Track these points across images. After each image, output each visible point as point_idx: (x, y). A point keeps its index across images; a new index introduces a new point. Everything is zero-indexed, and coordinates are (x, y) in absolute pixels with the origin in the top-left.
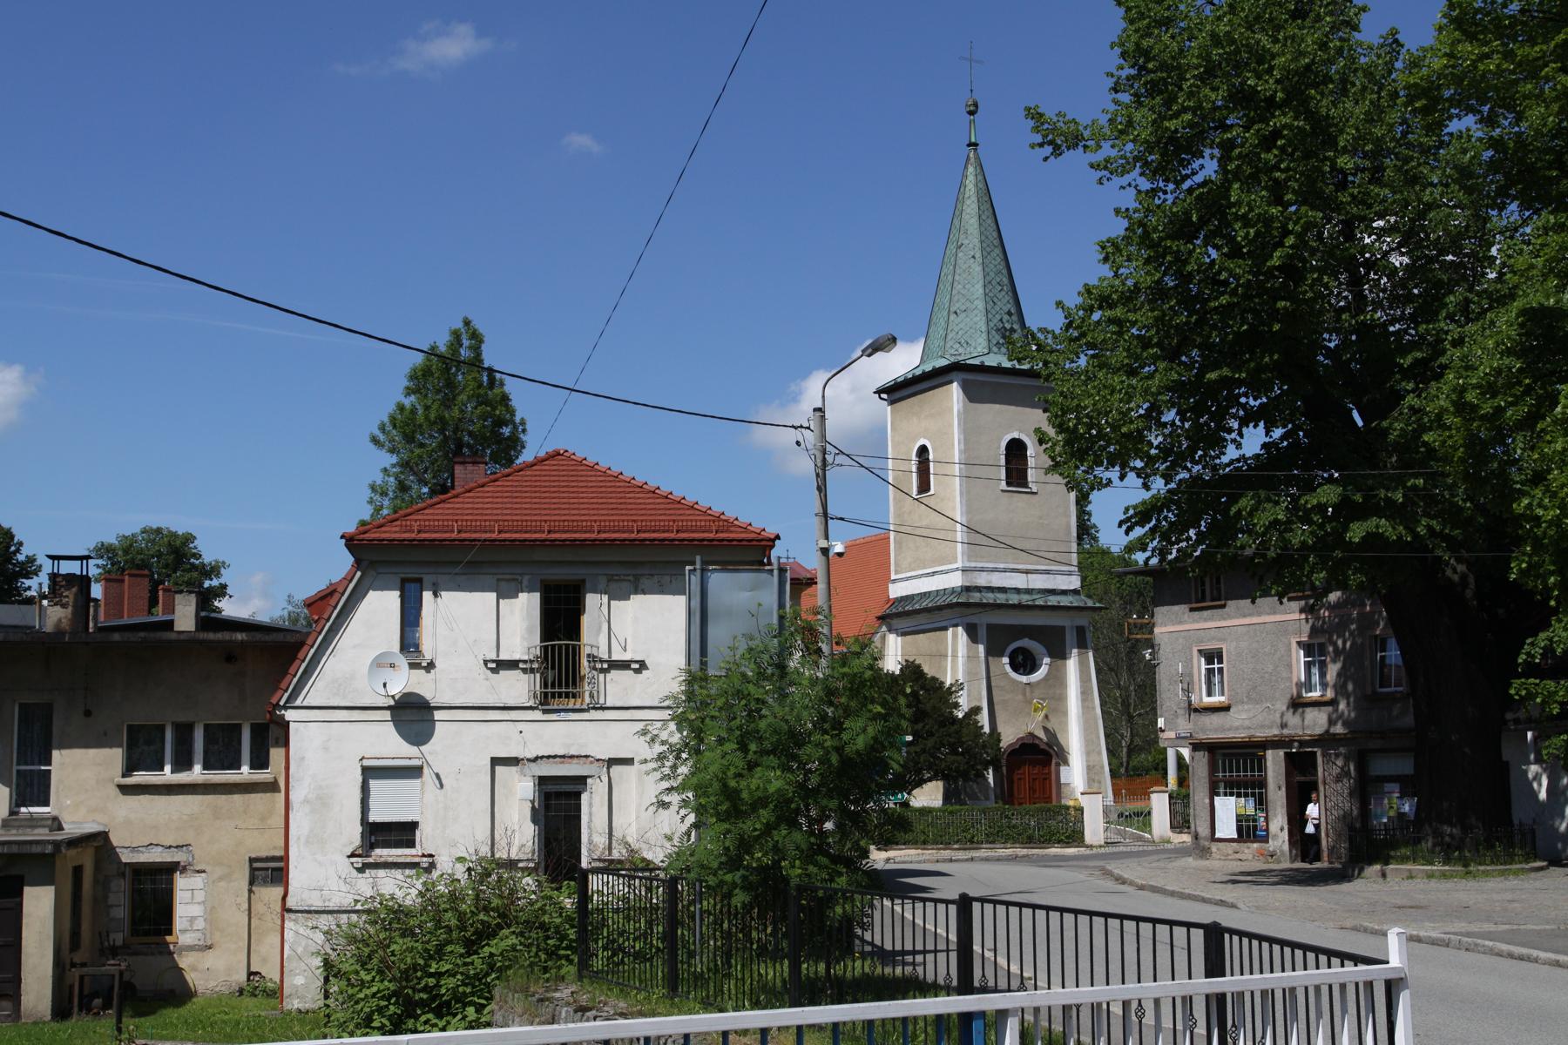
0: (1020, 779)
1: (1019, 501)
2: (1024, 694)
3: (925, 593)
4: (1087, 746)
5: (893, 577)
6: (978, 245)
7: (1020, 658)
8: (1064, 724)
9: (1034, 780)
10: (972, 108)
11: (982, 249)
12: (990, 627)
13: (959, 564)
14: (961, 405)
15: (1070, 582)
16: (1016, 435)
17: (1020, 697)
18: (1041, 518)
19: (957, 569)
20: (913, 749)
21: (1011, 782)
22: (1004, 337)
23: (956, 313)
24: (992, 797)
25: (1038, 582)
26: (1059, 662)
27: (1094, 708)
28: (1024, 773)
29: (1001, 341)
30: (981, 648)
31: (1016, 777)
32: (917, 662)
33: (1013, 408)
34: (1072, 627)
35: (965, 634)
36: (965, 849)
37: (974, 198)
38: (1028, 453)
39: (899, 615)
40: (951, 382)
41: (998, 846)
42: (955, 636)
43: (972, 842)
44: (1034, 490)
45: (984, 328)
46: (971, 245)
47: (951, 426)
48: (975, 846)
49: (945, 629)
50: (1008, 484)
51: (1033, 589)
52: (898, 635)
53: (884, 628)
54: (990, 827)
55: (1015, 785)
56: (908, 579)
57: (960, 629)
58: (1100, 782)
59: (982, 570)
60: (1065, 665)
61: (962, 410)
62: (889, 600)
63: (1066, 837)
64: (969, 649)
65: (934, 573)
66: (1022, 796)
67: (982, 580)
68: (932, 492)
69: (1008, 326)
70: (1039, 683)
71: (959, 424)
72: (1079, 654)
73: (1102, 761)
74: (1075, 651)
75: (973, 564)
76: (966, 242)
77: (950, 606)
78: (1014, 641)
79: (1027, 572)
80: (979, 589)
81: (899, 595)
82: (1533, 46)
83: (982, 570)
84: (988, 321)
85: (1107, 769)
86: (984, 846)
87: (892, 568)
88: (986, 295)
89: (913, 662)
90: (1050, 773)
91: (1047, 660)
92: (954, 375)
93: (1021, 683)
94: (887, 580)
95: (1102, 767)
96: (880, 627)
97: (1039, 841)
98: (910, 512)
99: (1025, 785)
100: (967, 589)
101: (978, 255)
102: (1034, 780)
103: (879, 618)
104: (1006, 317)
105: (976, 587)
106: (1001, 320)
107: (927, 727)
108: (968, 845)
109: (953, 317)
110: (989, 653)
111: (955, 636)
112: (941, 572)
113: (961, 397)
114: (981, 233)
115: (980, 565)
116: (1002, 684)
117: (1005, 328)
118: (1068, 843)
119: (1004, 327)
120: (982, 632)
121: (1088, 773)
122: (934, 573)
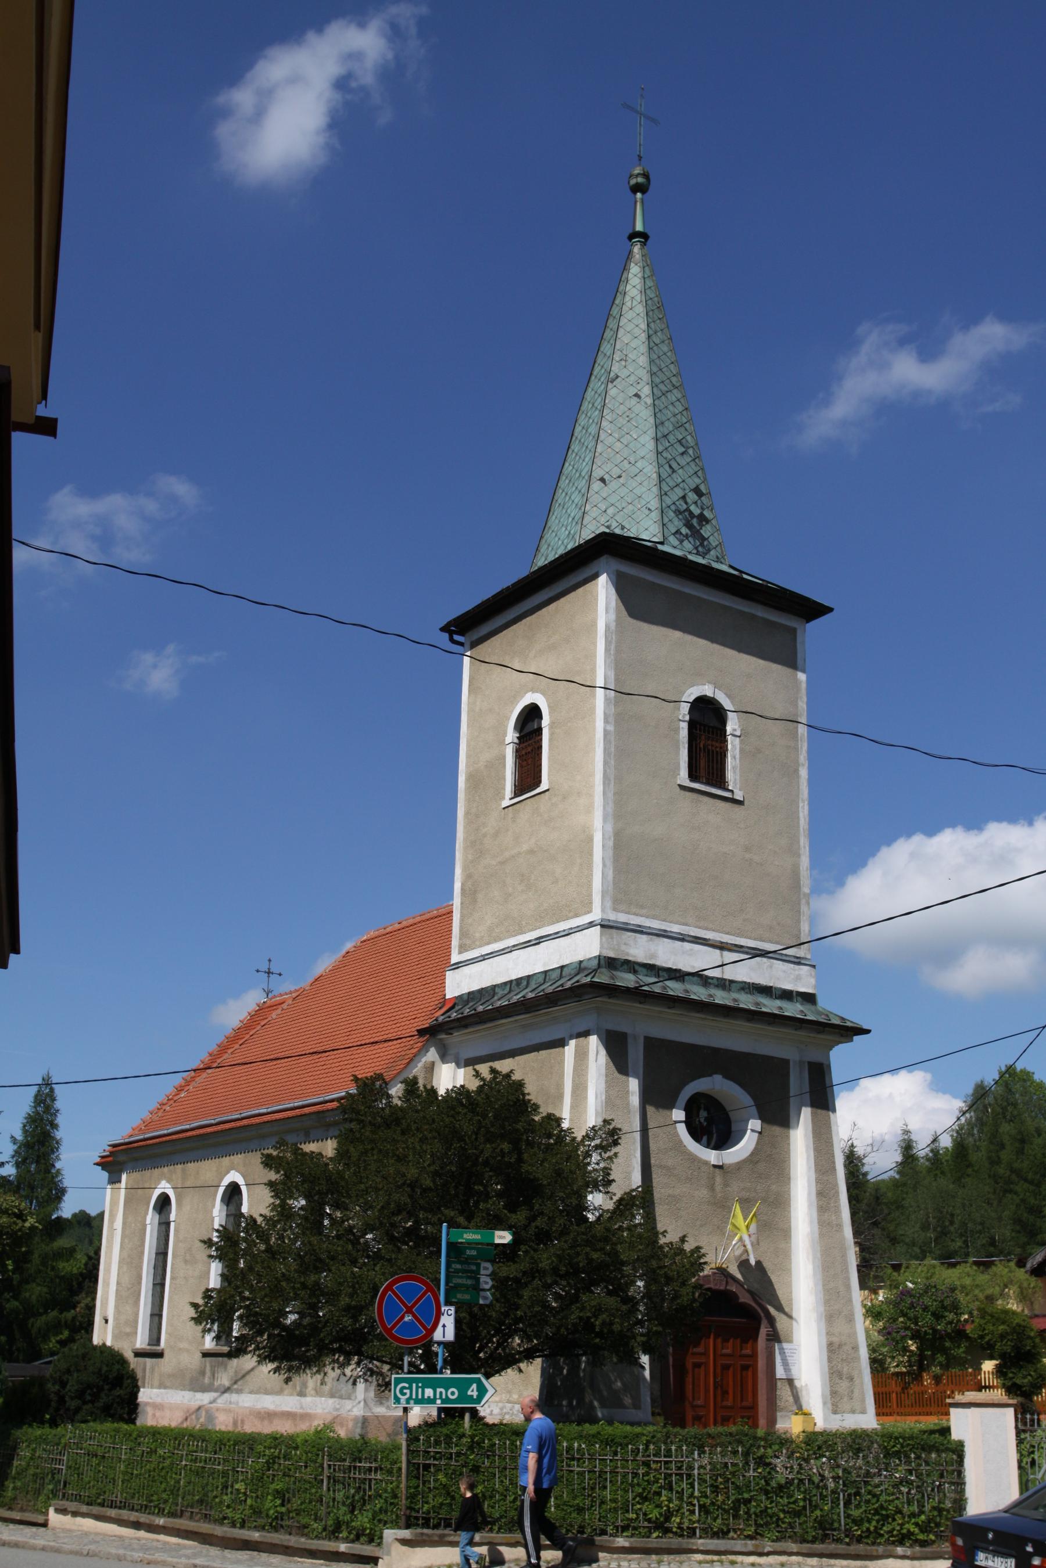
0: (697, 1365)
1: (710, 812)
2: (712, 1188)
3: (519, 981)
4: (827, 1302)
5: (455, 958)
6: (646, 377)
7: (703, 1114)
8: (785, 1255)
9: (726, 1368)
10: (640, 180)
11: (654, 385)
12: (652, 1045)
13: (596, 915)
14: (613, 616)
15: (798, 978)
16: (708, 690)
17: (703, 1193)
18: (747, 849)
19: (591, 924)
20: (509, 1270)
21: (681, 1371)
22: (688, 525)
23: (602, 480)
24: (646, 1399)
25: (747, 972)
26: (777, 1130)
27: (840, 1226)
28: (705, 1354)
29: (684, 531)
30: (634, 1084)
31: (690, 1361)
32: (516, 1077)
33: (702, 642)
34: (801, 1063)
35: (603, 1052)
36: (647, 1551)
37: (640, 309)
38: (729, 729)
39: (463, 1023)
40: (595, 576)
41: (739, 1545)
42: (581, 1056)
43: (661, 1526)
44: (738, 796)
45: (654, 504)
46: (633, 378)
47: (593, 656)
48: (675, 1542)
49: (561, 1043)
50: (693, 776)
51: (732, 982)
52: (458, 1066)
53: (432, 1054)
54: (715, 1489)
55: (689, 1379)
56: (484, 958)
57: (593, 1040)
58: (851, 1379)
59: (639, 930)
60: (788, 1137)
61: (613, 625)
62: (445, 1001)
63: (924, 1528)
64: (609, 1084)
65: (539, 941)
66: (699, 1402)
67: (639, 949)
68: (544, 785)
69: (696, 511)
70: (739, 1166)
71: (607, 650)
72: (814, 1116)
73: (853, 1335)
74: (806, 1113)
75: (622, 918)
76: (623, 374)
77: (577, 993)
78: (693, 1079)
79: (722, 947)
80: (631, 966)
81: (465, 990)
82: (487, 1202)
83: (639, 930)
84: (663, 494)
85: (864, 1353)
86: (700, 1543)
87: (455, 942)
88: (658, 453)
89: (508, 1076)
90: (754, 1355)
91: (755, 1124)
92: (604, 560)
93: (706, 1163)
94: (444, 964)
95: (855, 1348)
96: (424, 1050)
97: (848, 1533)
98: (496, 834)
99: (707, 1375)
100: (610, 963)
101: (646, 391)
102: (726, 1368)
103: (421, 1032)
104: (692, 497)
105: (627, 962)
106: (684, 498)
107: (540, 1222)
108: (654, 1540)
109: (596, 486)
110: (647, 1097)
111: (581, 1056)
112: (557, 936)
113: (613, 604)
114: (652, 362)
115: (635, 920)
116: (670, 1163)
117: (691, 513)
118: (923, 1544)
119: (688, 510)
120: (636, 1053)
121: (830, 1360)
122: (539, 941)
